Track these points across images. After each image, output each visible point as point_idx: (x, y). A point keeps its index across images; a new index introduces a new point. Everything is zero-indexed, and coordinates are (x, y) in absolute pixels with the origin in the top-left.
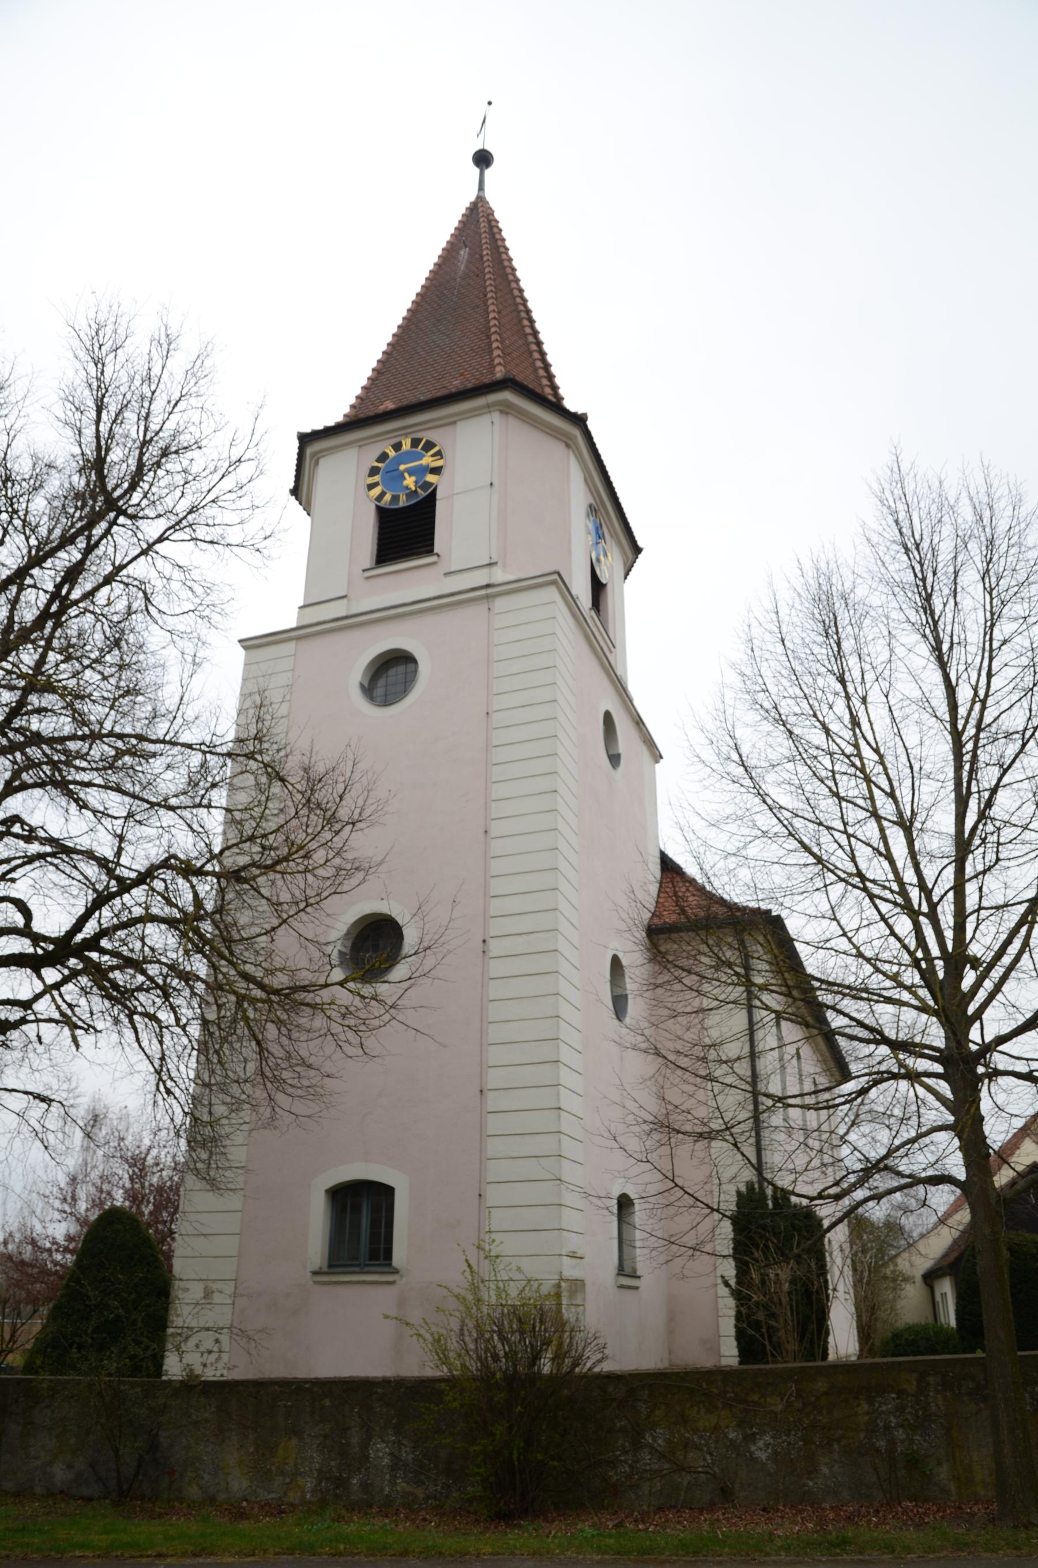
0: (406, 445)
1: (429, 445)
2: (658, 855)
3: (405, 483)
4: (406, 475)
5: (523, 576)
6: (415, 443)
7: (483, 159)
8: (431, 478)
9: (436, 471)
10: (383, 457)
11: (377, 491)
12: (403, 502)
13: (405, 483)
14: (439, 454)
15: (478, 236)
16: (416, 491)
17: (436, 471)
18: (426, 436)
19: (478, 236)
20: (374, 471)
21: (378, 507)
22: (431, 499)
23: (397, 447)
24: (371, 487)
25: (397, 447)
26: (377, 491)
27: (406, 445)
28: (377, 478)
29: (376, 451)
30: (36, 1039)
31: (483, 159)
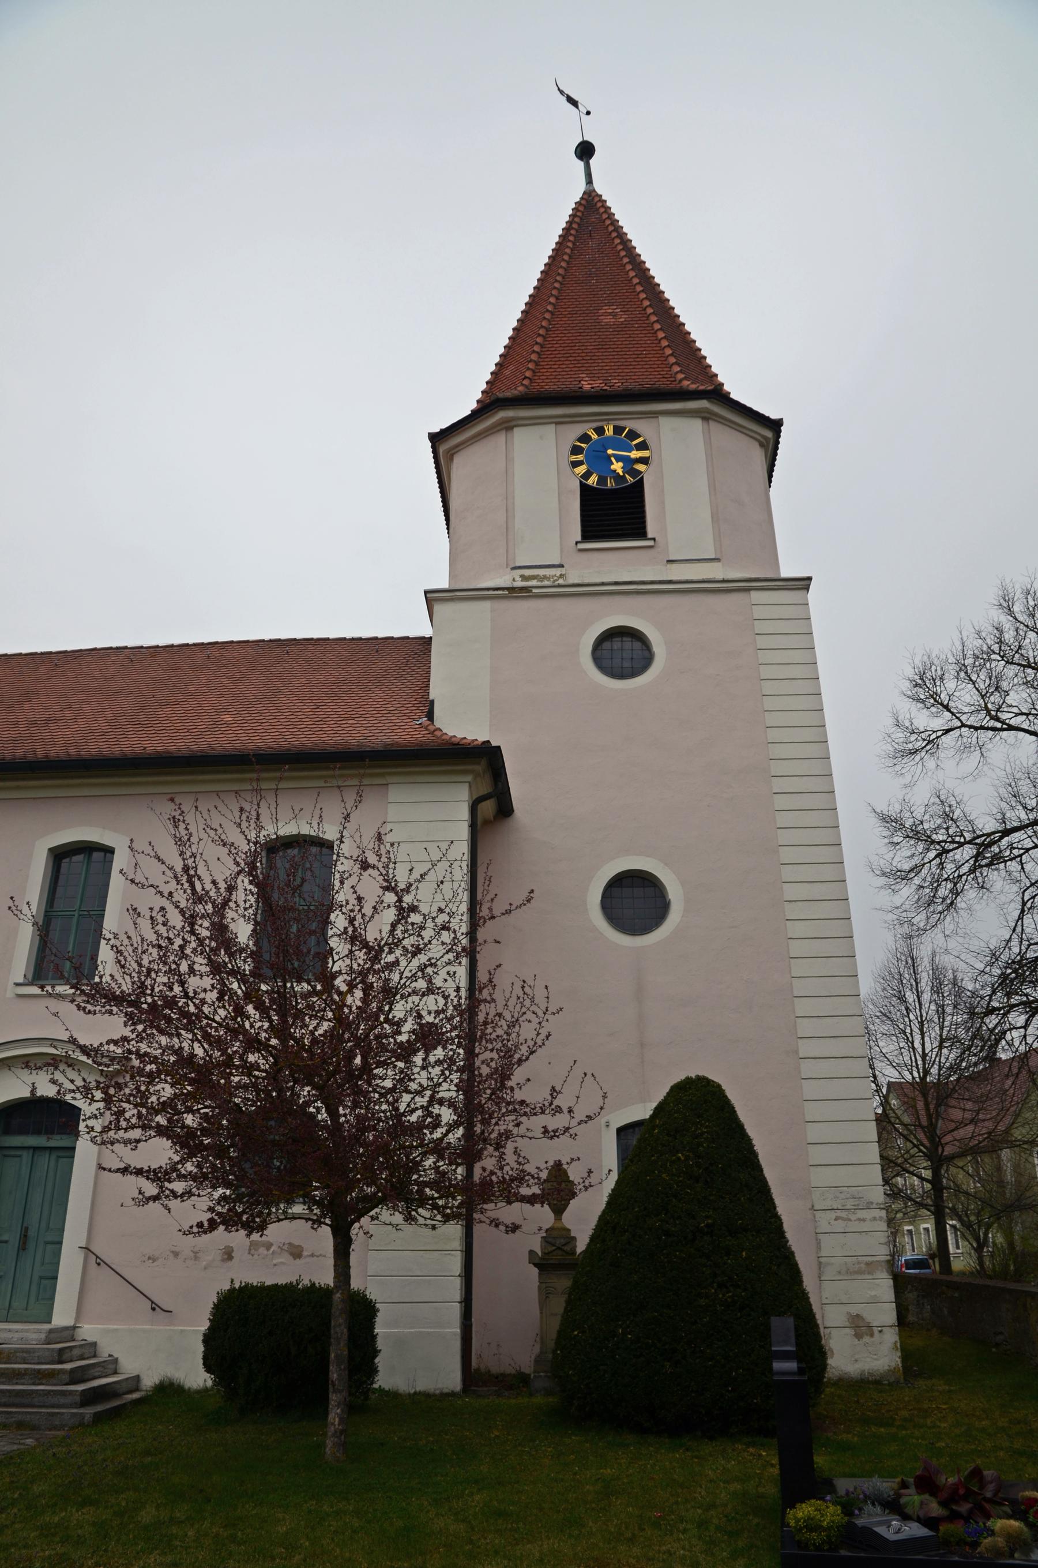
0: (609, 431)
1: (633, 435)
2: (874, 821)
3: (612, 467)
4: (613, 459)
5: (586, 581)
6: (618, 430)
7: (585, 151)
8: (641, 467)
9: (645, 461)
10: (585, 438)
11: (582, 469)
12: (610, 484)
13: (612, 467)
14: (643, 446)
15: (592, 226)
16: (624, 476)
17: (645, 461)
18: (630, 425)
19: (592, 226)
20: (576, 450)
21: (584, 488)
22: (639, 485)
23: (600, 431)
24: (575, 464)
25: (600, 431)
26: (582, 469)
27: (609, 431)
28: (580, 457)
29: (578, 430)
30: (31, 1245)
31: (585, 151)
